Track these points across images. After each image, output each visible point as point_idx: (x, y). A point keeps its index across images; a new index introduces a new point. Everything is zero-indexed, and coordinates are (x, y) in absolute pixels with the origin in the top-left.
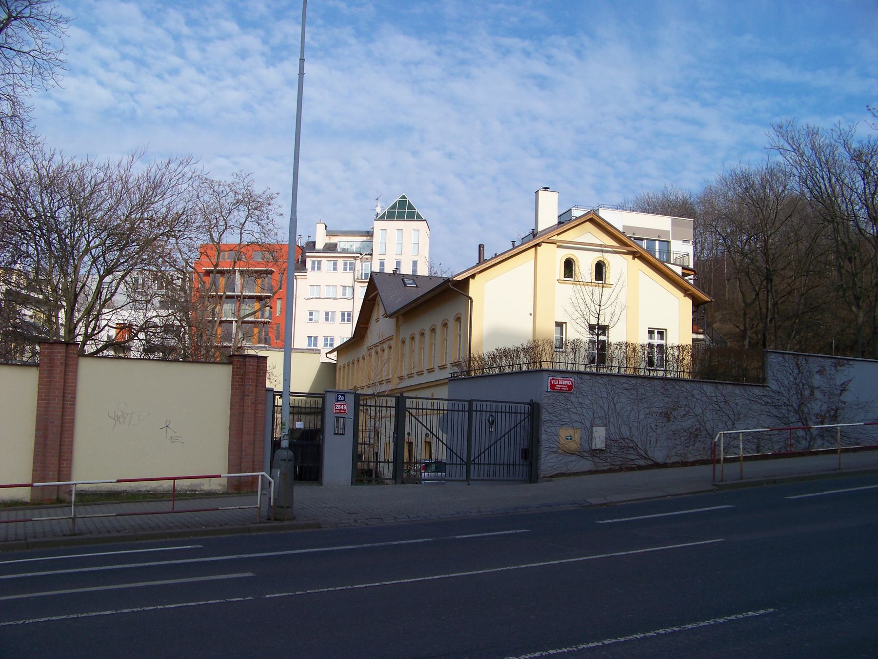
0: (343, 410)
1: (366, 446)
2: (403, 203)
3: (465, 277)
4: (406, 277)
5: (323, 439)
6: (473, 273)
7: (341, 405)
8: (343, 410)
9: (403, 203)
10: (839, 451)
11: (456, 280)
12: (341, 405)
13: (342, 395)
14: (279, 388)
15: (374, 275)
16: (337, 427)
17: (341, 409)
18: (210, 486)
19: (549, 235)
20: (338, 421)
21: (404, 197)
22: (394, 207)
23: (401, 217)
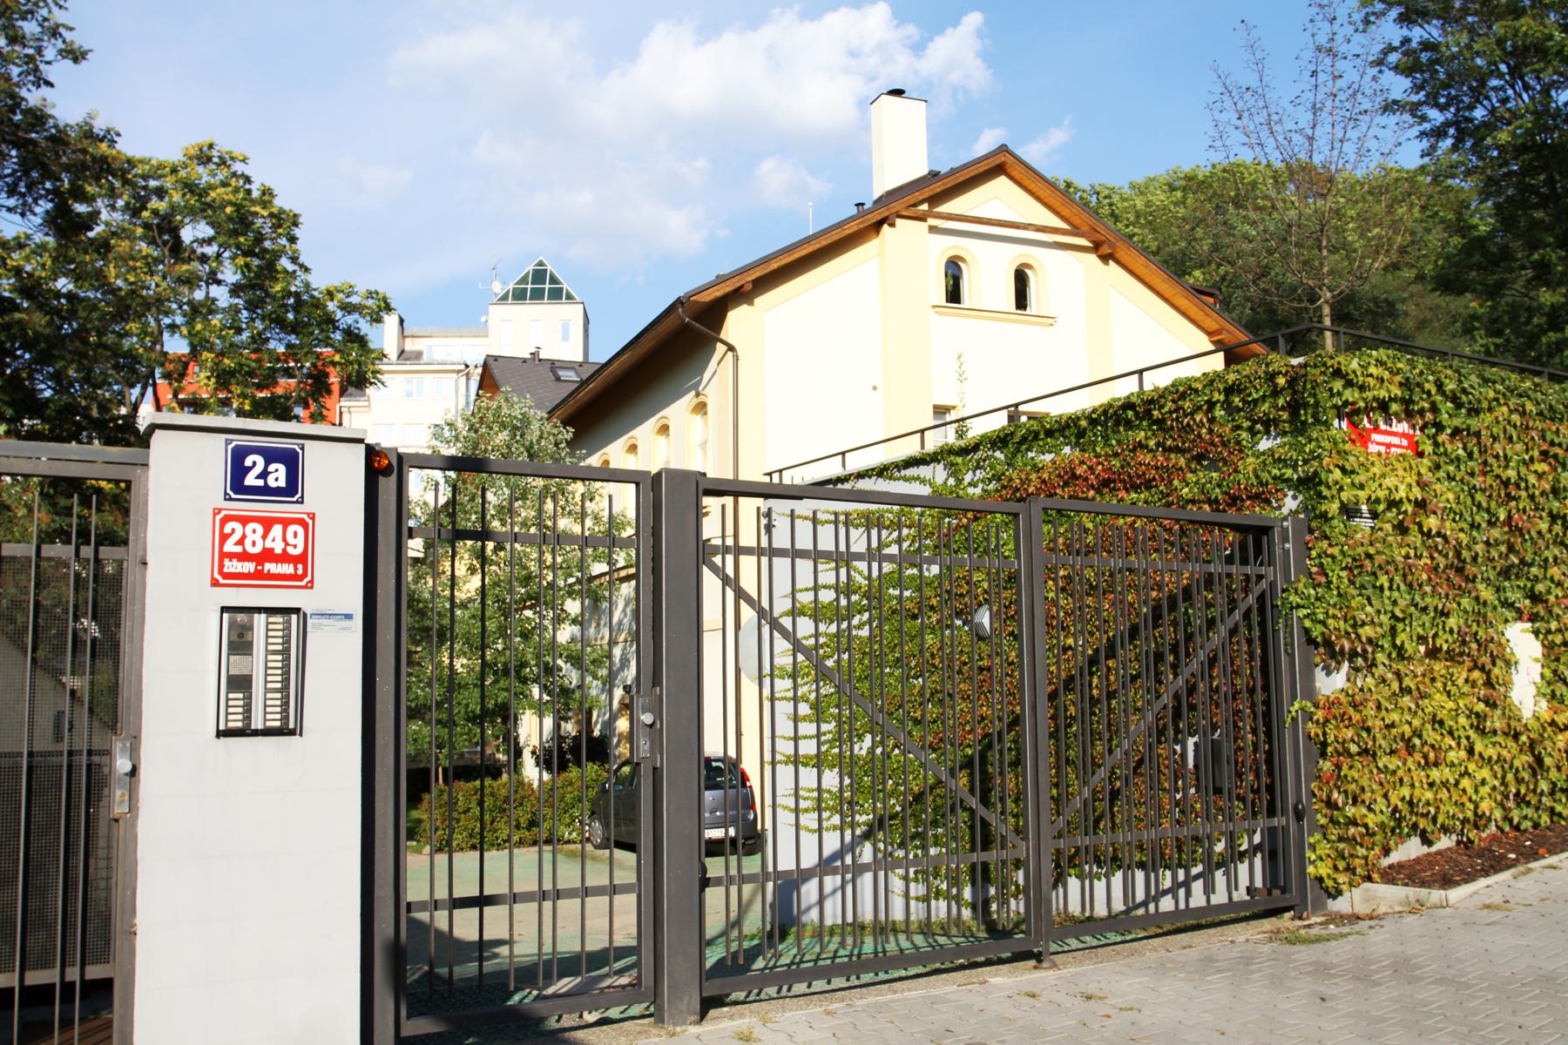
0: (284, 558)
1: (747, 889)
2: (539, 275)
3: (718, 294)
4: (557, 364)
5: (134, 772)
6: (737, 285)
7: (268, 524)
8: (284, 558)
9: (539, 275)
10: (1042, 436)
11: (697, 302)
12: (268, 524)
13: (271, 456)
14: (718, 542)
15: (491, 362)
16: (240, 683)
17: (267, 555)
18: (349, 617)
19: (911, 199)
20: (240, 643)
21: (541, 263)
22: (524, 280)
23: (537, 295)
